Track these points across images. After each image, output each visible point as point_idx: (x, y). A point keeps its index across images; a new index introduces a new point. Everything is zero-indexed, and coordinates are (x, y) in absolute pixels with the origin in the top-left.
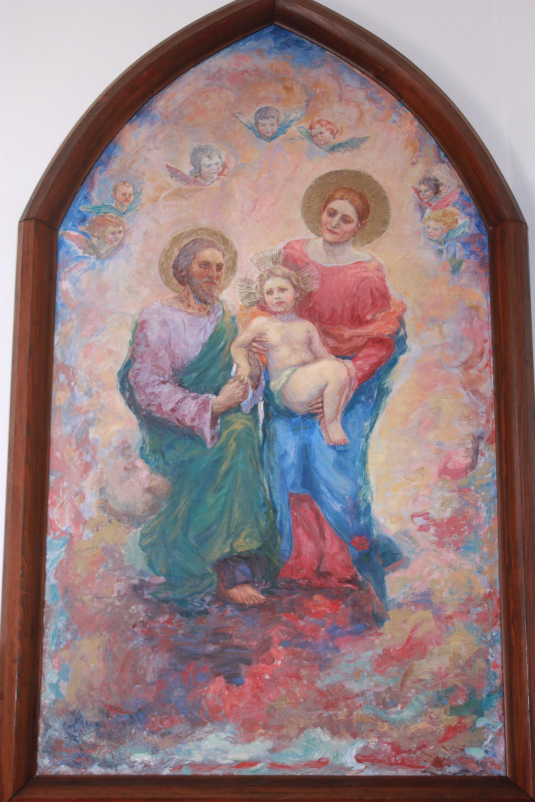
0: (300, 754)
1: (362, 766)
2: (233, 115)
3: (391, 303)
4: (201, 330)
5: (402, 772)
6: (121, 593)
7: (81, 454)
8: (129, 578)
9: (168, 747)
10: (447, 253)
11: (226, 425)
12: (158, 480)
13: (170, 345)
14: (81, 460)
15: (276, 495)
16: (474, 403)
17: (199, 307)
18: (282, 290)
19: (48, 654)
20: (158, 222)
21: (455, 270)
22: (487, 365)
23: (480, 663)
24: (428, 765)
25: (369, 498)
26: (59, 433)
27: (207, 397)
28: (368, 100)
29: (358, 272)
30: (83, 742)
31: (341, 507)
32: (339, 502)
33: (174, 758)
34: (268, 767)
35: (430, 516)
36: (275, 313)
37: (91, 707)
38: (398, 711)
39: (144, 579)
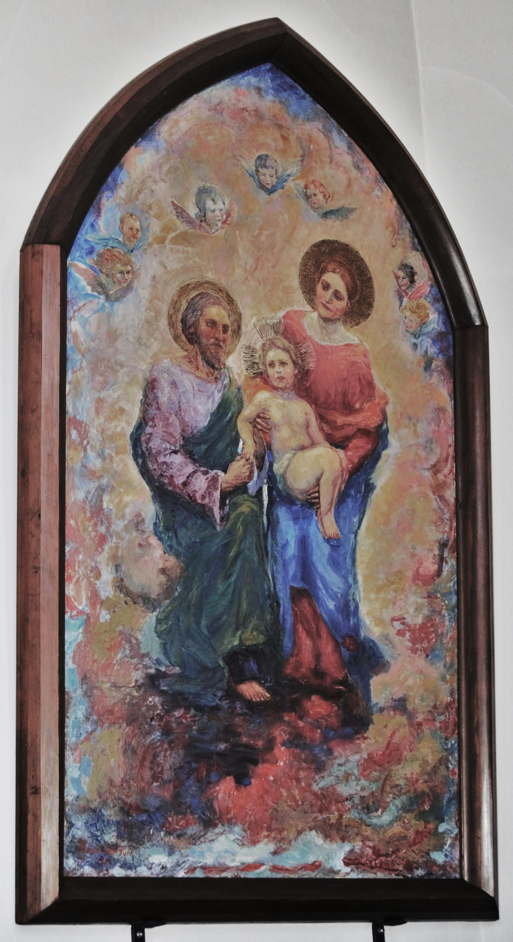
0: (298, 857)
1: (348, 869)
2: (235, 157)
3: (376, 394)
4: (209, 397)
5: (380, 875)
6: (139, 683)
7: (96, 525)
8: (146, 667)
9: (183, 848)
10: (421, 348)
11: (235, 506)
12: (172, 561)
13: (180, 410)
14: (96, 531)
15: (279, 587)
16: (440, 509)
17: (207, 371)
18: (283, 363)
19: (69, 746)
20: (165, 267)
21: (427, 367)
22: (451, 471)
23: (443, 771)
24: (401, 868)
25: (357, 598)
26: (73, 499)
27: (216, 473)
28: (355, 167)
29: (349, 356)
30: (105, 842)
31: (335, 606)
32: (333, 599)
33: (188, 860)
34: (270, 870)
35: (406, 620)
36: (276, 389)
37: (111, 805)
38: (379, 816)
39: (160, 669)
